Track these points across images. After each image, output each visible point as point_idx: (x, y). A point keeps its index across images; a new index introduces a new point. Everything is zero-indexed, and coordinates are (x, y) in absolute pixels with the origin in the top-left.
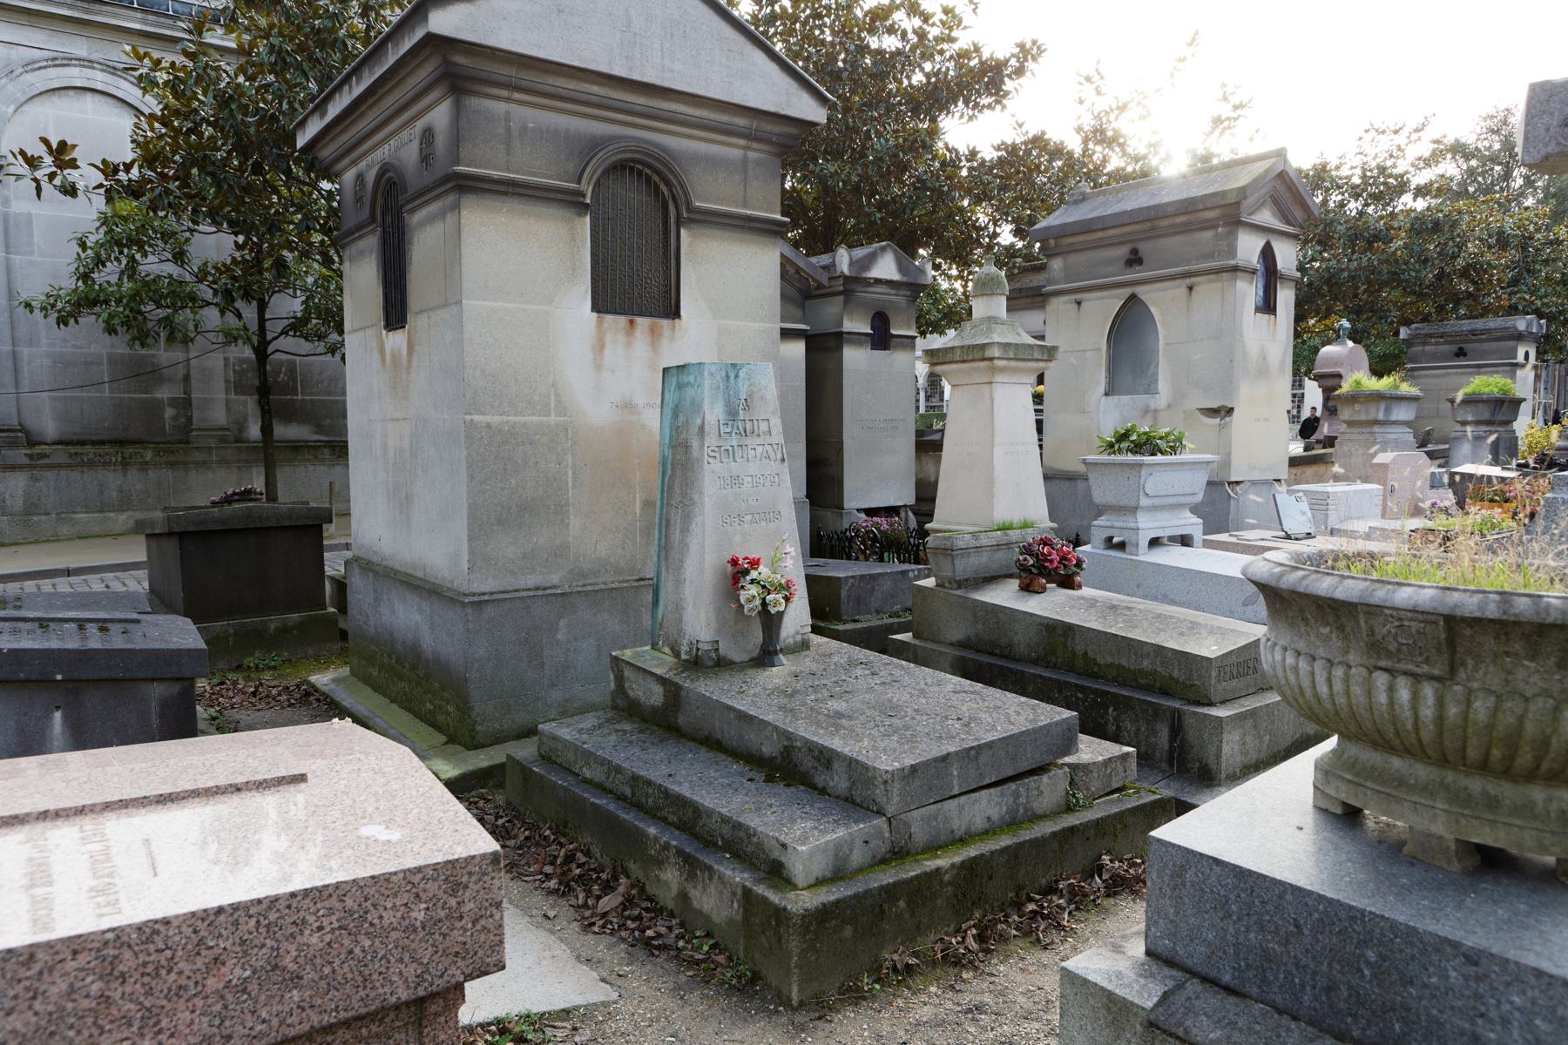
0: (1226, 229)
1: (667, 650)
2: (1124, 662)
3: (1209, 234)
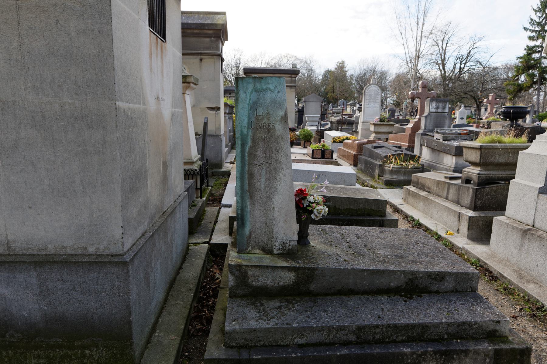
0: (215, 39)
1: (257, 251)
2: (352, 207)
3: (208, 40)
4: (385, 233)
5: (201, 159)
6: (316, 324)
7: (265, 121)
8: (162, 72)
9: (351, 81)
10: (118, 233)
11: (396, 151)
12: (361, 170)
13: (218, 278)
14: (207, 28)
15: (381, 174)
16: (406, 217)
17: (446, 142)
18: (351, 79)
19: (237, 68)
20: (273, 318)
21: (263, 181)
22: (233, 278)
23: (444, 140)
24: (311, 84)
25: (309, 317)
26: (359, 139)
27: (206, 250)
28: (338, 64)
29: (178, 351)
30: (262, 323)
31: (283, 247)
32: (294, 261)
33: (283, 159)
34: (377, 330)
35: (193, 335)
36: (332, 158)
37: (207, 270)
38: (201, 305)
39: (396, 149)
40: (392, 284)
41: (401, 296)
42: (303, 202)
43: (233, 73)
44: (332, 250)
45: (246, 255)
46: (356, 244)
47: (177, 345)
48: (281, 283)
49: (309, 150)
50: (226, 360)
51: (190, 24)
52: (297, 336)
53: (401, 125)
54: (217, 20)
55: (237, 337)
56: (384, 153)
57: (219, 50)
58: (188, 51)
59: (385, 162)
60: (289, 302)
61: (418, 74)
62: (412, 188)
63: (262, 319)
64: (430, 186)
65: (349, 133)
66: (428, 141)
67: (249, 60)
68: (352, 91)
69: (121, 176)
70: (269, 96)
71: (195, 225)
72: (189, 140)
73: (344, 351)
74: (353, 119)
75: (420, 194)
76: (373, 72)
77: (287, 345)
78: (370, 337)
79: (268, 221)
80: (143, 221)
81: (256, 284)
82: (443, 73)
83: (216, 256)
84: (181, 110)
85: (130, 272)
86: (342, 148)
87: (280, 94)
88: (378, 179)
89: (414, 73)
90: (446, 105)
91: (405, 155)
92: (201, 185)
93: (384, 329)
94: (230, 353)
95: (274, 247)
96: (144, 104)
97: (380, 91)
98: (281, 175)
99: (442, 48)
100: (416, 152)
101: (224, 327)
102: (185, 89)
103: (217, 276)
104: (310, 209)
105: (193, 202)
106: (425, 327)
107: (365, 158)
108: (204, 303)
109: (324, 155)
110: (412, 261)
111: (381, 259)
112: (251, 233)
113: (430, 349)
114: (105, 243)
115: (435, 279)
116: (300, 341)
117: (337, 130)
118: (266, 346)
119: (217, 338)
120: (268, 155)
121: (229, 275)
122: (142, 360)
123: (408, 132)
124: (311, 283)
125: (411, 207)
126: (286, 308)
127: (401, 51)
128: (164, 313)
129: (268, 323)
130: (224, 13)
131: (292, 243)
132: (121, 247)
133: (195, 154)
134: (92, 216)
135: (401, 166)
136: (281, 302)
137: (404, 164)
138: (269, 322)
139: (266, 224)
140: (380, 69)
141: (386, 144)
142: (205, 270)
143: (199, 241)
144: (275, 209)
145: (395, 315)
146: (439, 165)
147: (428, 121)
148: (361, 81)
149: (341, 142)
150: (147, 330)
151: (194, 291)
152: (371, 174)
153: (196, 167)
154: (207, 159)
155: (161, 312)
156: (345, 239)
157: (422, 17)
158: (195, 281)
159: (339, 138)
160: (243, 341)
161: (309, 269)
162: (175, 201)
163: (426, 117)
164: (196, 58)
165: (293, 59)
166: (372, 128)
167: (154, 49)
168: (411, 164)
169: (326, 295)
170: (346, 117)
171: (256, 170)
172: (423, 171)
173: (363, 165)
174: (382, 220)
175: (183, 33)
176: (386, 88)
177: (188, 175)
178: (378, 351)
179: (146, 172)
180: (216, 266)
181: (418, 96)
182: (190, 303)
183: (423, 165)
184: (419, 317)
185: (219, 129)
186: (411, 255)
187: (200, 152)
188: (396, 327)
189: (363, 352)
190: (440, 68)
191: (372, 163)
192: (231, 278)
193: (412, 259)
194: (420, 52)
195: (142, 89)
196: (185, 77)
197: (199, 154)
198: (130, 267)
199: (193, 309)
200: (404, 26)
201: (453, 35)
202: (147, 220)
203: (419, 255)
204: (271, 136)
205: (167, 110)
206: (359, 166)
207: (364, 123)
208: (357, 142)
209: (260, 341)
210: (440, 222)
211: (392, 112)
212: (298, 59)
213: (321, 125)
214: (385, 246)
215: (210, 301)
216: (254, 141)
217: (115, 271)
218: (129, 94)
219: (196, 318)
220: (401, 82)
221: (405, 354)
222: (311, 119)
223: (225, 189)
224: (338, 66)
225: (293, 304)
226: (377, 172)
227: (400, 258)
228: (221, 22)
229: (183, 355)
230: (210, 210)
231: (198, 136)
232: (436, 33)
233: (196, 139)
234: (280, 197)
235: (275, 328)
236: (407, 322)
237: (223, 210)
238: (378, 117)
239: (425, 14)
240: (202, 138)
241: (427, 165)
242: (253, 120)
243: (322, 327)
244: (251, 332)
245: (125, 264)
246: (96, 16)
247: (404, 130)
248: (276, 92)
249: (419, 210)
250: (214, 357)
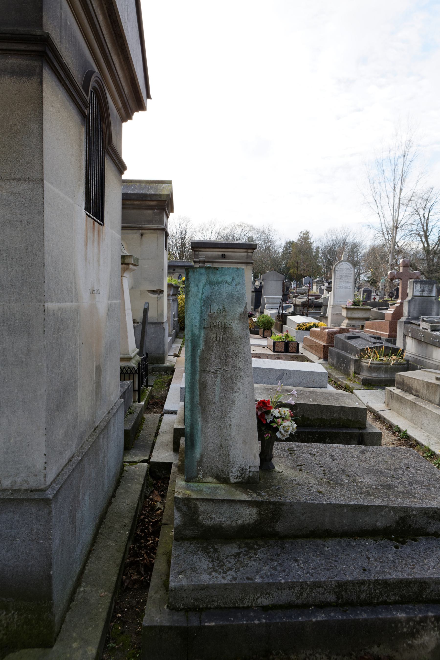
0: (158, 211)
1: (210, 479)
2: (324, 417)
3: (150, 212)
4: (366, 454)
5: (140, 354)
6: (284, 578)
7: (220, 319)
8: (98, 261)
9: (317, 254)
10: (40, 462)
11: (374, 343)
12: (333, 365)
13: (159, 509)
14: (149, 199)
15: (357, 372)
16: (390, 427)
17: (435, 333)
18: (318, 252)
19: (183, 239)
20: (230, 569)
21: (217, 391)
22: (179, 515)
23: (432, 330)
24: (270, 256)
25: (276, 570)
26: (329, 326)
27: (145, 472)
28: (302, 235)
29: (109, 613)
30: (216, 577)
31: (242, 474)
32: (256, 492)
33: (241, 365)
34: (363, 588)
35: (127, 587)
36: (297, 352)
37: (146, 497)
38: (137, 547)
39: (374, 340)
40: (378, 524)
41: (391, 539)
42: (266, 417)
43: (178, 245)
44: (302, 477)
45: (196, 484)
46: (332, 469)
47: (108, 605)
48: (240, 522)
49: (270, 341)
50: (170, 628)
51: (130, 194)
52: (261, 595)
53: (379, 309)
54: (162, 190)
55: (185, 596)
56: (360, 345)
57: (162, 223)
58: (128, 225)
59: (361, 357)
60: (251, 548)
61: (396, 247)
62: (396, 390)
63: (216, 571)
64: (418, 388)
65: (317, 319)
66: (413, 330)
67: (197, 230)
68: (318, 266)
69: (47, 392)
70: (225, 290)
71: (132, 439)
72: (126, 331)
73: (321, 617)
74: (320, 301)
75: (406, 398)
76: (343, 244)
77: (248, 608)
78: (354, 597)
79: (224, 441)
80: (70, 443)
81: (208, 523)
82: (426, 245)
83: (156, 478)
84: (118, 301)
85: (53, 513)
86: (308, 337)
87: (238, 288)
88: (354, 377)
89: (392, 247)
90: (432, 288)
91: (386, 348)
92: (140, 386)
93: (371, 586)
94: (176, 618)
95: (231, 474)
96: (77, 301)
98: (239, 384)
99: (424, 217)
100: (399, 344)
101: (168, 580)
102: (124, 271)
103: (159, 505)
104: (275, 425)
105: (129, 408)
106: (423, 584)
107: (337, 350)
108: (142, 543)
109: (288, 349)
110: (403, 493)
111: (364, 490)
112: (202, 457)
113: (430, 614)
114: (23, 475)
115: (433, 517)
116: (265, 601)
117: (302, 314)
118: (221, 608)
119: (159, 596)
120: (224, 359)
121: (175, 511)
122: (63, 626)
123: (388, 319)
124: (277, 522)
125: (395, 414)
126: (245, 555)
127: (375, 220)
128: (92, 559)
129: (224, 578)
130: (170, 182)
131: (253, 469)
132: (43, 479)
133: (132, 348)
134: (9, 441)
135: (381, 362)
136: (240, 548)
137: (385, 359)
138: (225, 575)
139: (221, 445)
140: (351, 240)
141: (362, 333)
142: (143, 498)
143: (136, 459)
144: (232, 426)
145: (384, 567)
146: (427, 361)
147: (412, 307)
148: (329, 254)
149: (308, 329)
150: (70, 584)
151: (129, 528)
152: (345, 371)
153: (133, 364)
154: (147, 354)
155: (88, 557)
156: (318, 462)
157: (400, 182)
158: (130, 514)
159: (304, 324)
160: (192, 601)
161: (274, 503)
162: (109, 412)
163: (409, 301)
164: (136, 233)
165: (248, 229)
166: (344, 313)
167: (90, 234)
168: (393, 360)
169: (296, 537)
170: (312, 298)
171: (209, 379)
172: (407, 369)
173: (335, 360)
174: (362, 433)
175: (123, 204)
176: (359, 263)
177: (125, 374)
178: (365, 616)
179: (76, 382)
180: (156, 492)
181: (399, 276)
182: (124, 544)
183: (408, 361)
184: (415, 570)
185: (162, 315)
186: (401, 484)
187: (139, 343)
188: (386, 583)
189: (345, 618)
190: (422, 240)
191: (345, 358)
192: (177, 515)
193: (402, 490)
194: (399, 222)
195: (75, 283)
196: (123, 257)
197: (137, 348)
198: (53, 506)
199: (127, 552)
200: (378, 193)
201: (435, 202)
202: (76, 441)
203: (411, 484)
204: (228, 337)
205: (102, 303)
206: (330, 360)
207: (334, 306)
208: (327, 330)
209: (213, 601)
210: (432, 435)
211: (368, 293)
212: (254, 229)
213: (284, 308)
214: (368, 472)
215: (149, 541)
216: (207, 343)
217: (34, 510)
218: (60, 292)
219: (131, 564)
220: (377, 256)
221: (400, 621)
222: (270, 300)
223: (168, 390)
224: (302, 238)
225: (255, 550)
226: (352, 368)
227: (387, 489)
228: (166, 192)
229: (114, 617)
230: (151, 417)
231: (136, 324)
232: (416, 200)
233: (134, 328)
234: (238, 411)
235: (233, 584)
236: (400, 576)
237: (167, 418)
238: (351, 300)
239: (403, 178)
240: (141, 326)
241: (413, 360)
242: (206, 317)
243: (293, 583)
244: (202, 589)
245: (47, 502)
246: (26, 205)
247: (382, 317)
248: (234, 284)
249: (406, 418)
250: (155, 624)
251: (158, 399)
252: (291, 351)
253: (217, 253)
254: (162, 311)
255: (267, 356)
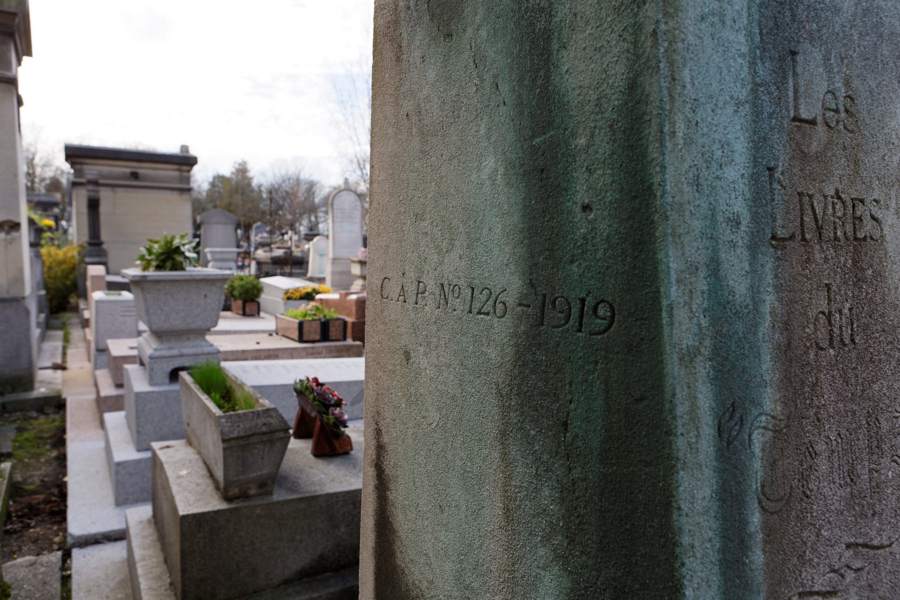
18: (260, 191)
97: (358, 203)
159: (297, 290)
185: (20, 279)
222: (218, 256)
251: (35, 492)
252: (334, 338)
253: (123, 168)
254: (21, 271)
255: (290, 354)
